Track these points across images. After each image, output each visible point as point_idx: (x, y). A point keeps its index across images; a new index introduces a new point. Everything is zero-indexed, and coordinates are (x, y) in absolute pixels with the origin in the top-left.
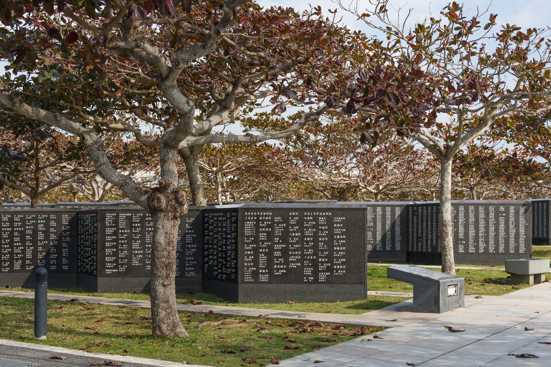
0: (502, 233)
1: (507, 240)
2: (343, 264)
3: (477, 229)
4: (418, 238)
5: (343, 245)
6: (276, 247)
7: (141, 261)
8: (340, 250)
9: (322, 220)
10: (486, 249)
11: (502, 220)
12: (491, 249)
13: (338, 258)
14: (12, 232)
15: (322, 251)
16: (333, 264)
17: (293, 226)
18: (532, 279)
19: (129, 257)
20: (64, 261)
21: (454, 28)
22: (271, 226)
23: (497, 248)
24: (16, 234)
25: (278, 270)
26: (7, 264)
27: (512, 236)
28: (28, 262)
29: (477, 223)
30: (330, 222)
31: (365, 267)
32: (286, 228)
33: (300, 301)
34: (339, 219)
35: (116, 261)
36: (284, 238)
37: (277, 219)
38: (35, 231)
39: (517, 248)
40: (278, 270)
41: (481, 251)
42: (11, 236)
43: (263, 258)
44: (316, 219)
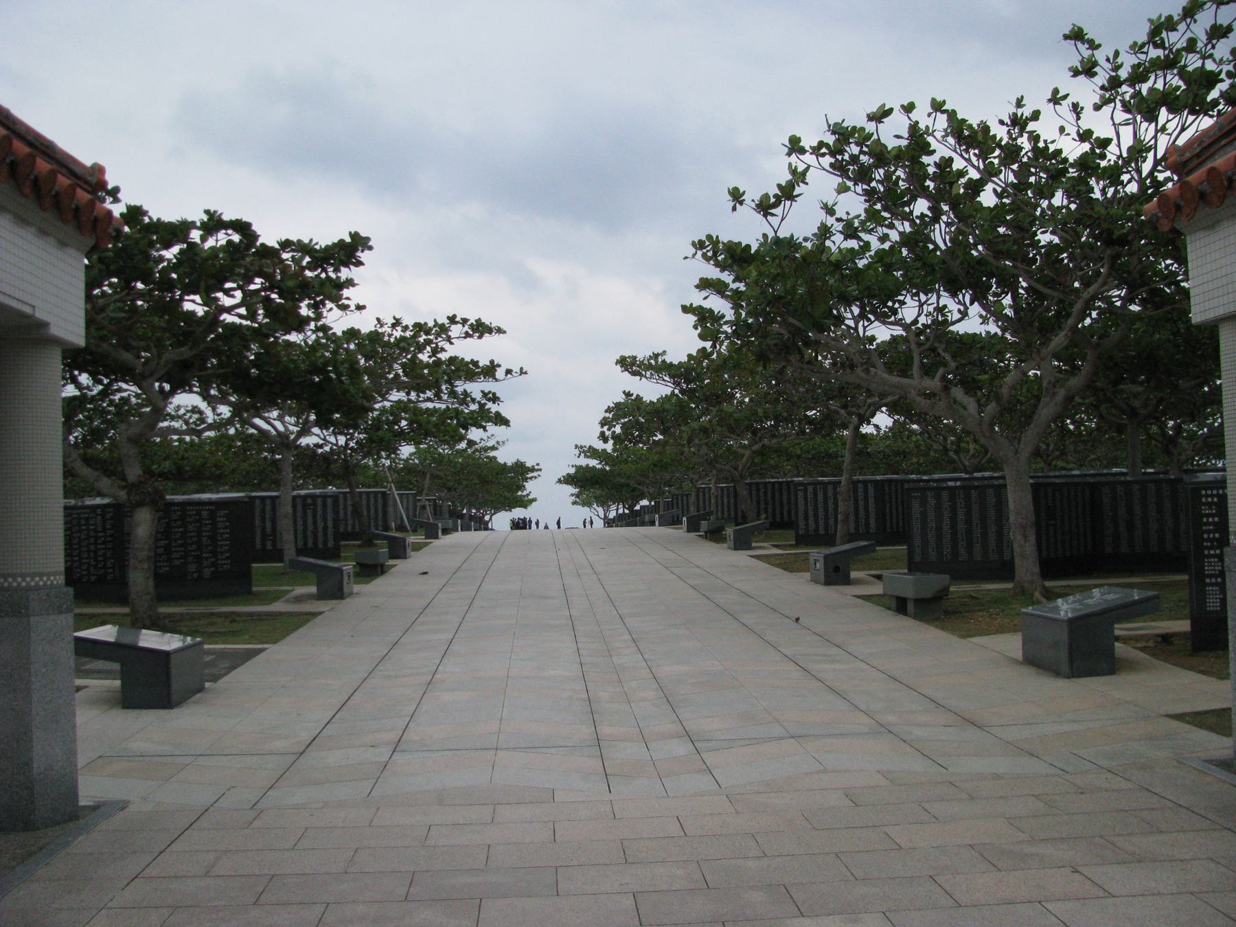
0: (310, 527)
1: (315, 533)
2: (227, 558)
5: (226, 539)
9: (205, 514)
11: (310, 512)
13: (222, 553)
17: (175, 521)
21: (886, 829)
34: (223, 513)
44: (198, 513)
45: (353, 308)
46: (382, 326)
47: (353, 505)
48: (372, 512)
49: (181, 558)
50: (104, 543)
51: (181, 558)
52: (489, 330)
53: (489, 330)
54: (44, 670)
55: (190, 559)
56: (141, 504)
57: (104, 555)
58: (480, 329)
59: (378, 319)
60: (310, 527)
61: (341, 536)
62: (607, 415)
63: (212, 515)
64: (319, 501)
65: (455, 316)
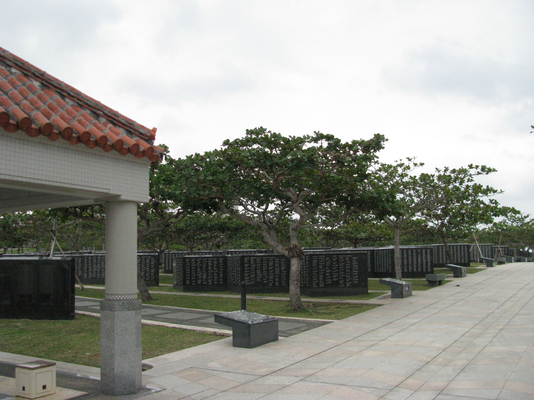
0: (420, 262)
1: (422, 265)
2: (357, 278)
3: (408, 261)
4: (379, 265)
5: (357, 270)
6: (327, 271)
7: (261, 279)
8: (356, 272)
10: (412, 270)
12: (415, 270)
13: (355, 276)
14: (196, 267)
15: (348, 273)
16: (353, 279)
17: (334, 262)
18: (438, 283)
19: (255, 277)
20: (221, 280)
22: (325, 262)
23: (417, 270)
24: (198, 267)
25: (328, 281)
26: (194, 281)
27: (424, 264)
28: (204, 280)
29: (408, 258)
30: (351, 259)
31: (367, 280)
32: (331, 263)
33: (256, 293)
34: (355, 258)
35: (250, 279)
36: (331, 267)
37: (327, 259)
38: (207, 266)
39: (427, 269)
40: (328, 281)
41: (410, 271)
42: (196, 268)
43: (321, 277)
44: (344, 258)
45: (418, 165)
46: (439, 171)
47: (446, 252)
48: (462, 254)
49: (337, 277)
50: (305, 270)
51: (337, 277)
52: (490, 170)
53: (490, 170)
54: (121, 333)
56: (293, 257)
57: (305, 276)
58: (487, 170)
59: (437, 169)
60: (420, 262)
61: (433, 265)
64: (424, 250)
65: (472, 165)
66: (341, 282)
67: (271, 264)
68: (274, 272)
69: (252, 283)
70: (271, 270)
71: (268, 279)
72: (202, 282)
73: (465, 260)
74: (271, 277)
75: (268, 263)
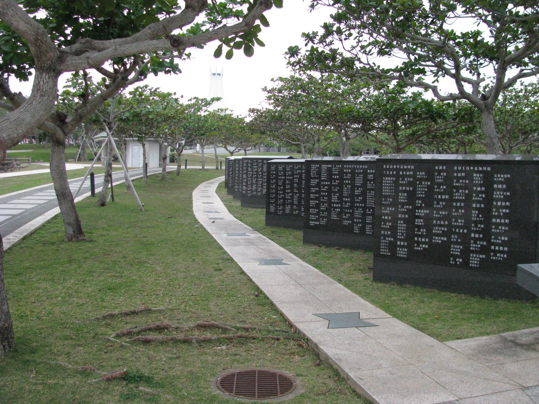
9: (477, 178)
14: (285, 180)
25: (419, 243)
32: (430, 188)
34: (501, 177)
37: (421, 174)
40: (419, 243)
42: (284, 184)
49: (443, 234)
51: (443, 234)
55: (454, 238)
62: (130, 33)
63: (488, 182)
66: (456, 250)
67: (359, 181)
68: (364, 201)
69: (323, 222)
70: (358, 196)
71: (352, 217)
72: (292, 210)
73: (382, 252)
74: (358, 213)
75: (353, 179)
